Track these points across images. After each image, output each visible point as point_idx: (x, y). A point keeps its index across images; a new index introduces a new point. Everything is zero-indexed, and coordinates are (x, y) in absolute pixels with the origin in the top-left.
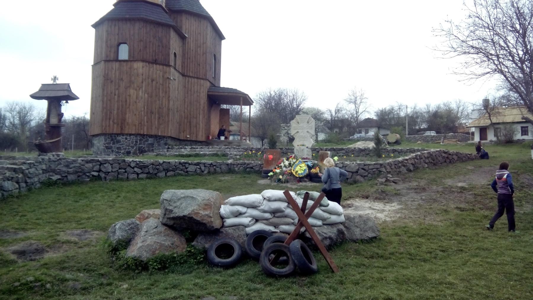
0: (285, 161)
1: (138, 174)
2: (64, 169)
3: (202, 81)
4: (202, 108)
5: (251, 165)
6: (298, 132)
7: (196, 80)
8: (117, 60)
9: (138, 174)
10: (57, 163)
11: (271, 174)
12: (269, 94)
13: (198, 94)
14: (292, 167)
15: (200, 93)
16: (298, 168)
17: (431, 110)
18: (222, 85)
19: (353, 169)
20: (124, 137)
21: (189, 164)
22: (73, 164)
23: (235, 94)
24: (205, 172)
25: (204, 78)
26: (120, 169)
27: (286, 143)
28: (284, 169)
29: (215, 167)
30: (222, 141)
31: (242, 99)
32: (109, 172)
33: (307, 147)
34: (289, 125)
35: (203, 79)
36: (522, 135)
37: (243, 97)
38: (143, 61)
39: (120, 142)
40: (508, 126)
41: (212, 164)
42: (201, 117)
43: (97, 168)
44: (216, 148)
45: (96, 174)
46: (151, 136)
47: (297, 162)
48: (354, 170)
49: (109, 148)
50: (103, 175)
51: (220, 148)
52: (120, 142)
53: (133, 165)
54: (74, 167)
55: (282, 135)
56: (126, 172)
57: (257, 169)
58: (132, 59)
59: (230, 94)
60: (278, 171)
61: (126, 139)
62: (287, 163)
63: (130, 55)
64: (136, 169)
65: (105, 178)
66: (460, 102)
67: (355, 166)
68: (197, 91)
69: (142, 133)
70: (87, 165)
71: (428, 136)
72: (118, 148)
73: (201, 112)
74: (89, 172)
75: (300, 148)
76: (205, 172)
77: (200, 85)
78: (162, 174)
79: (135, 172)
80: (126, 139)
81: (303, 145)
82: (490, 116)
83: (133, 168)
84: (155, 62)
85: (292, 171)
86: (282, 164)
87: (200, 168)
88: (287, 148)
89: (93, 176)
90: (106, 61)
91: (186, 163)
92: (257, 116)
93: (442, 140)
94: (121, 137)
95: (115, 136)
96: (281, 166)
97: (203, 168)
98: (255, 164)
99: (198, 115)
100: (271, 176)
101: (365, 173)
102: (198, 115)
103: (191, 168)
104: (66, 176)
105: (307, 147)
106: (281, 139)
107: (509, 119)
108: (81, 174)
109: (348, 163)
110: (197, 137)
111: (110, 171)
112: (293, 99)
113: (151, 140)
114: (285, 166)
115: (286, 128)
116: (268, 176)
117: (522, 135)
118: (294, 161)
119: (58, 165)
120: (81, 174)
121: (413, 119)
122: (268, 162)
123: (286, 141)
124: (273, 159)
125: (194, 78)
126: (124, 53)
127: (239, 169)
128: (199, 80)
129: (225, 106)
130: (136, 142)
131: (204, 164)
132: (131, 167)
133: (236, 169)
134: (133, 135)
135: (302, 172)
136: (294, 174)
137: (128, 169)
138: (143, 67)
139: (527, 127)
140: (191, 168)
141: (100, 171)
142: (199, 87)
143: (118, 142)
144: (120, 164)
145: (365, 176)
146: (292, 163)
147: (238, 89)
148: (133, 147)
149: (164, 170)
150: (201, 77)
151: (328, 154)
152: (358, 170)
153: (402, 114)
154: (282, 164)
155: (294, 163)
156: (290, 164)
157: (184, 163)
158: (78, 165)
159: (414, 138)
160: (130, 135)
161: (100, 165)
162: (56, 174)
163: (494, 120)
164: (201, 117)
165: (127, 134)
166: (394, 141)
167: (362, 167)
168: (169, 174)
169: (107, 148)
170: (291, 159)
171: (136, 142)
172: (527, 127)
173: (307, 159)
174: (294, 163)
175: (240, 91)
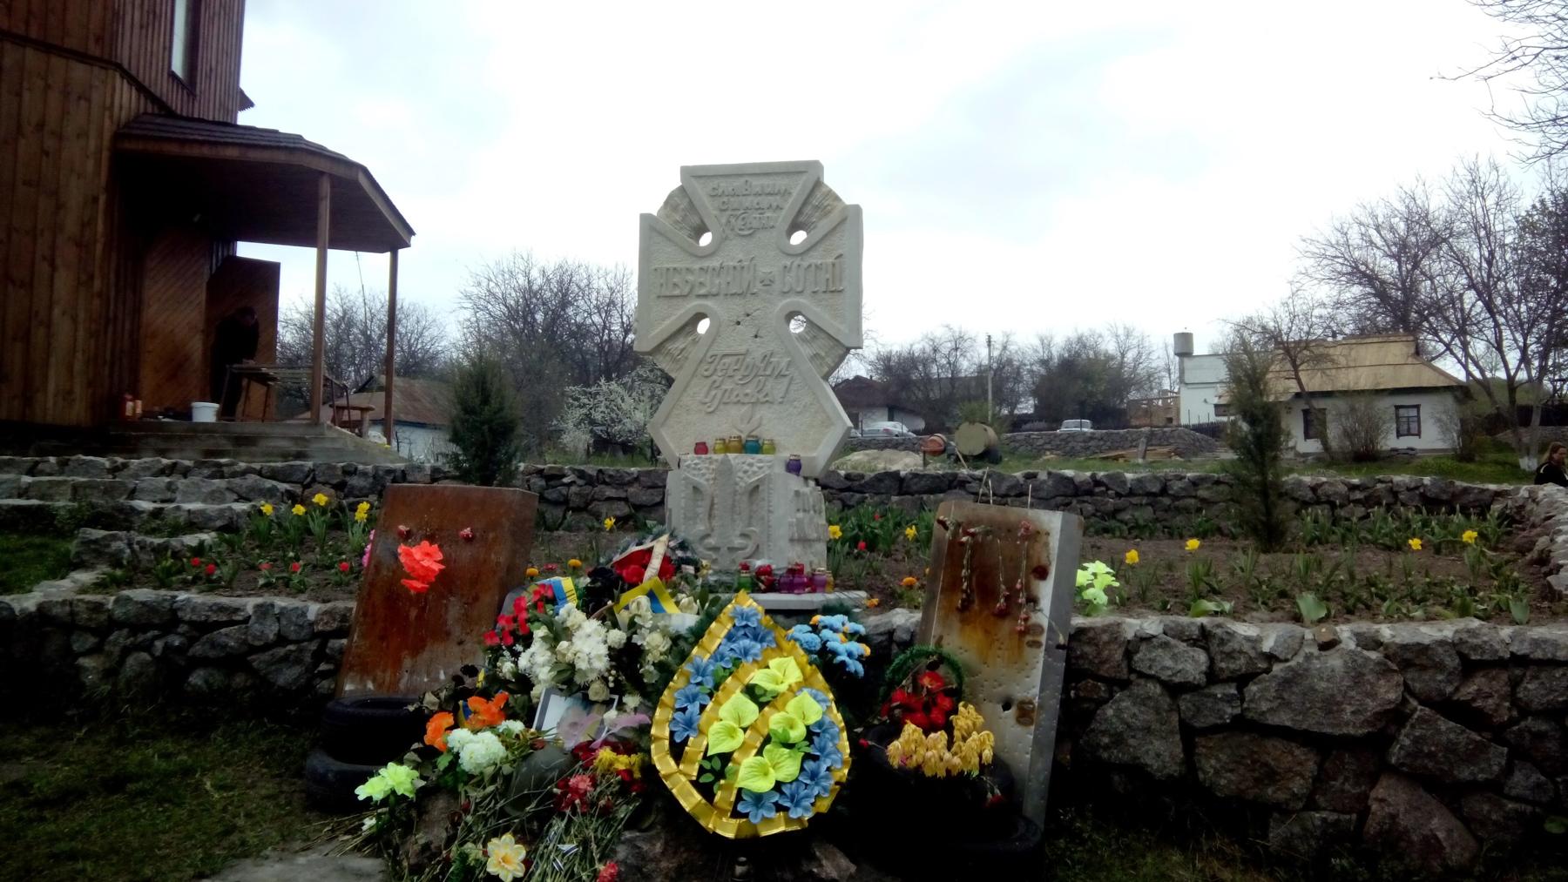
0: (569, 612)
3: (79, 71)
4: (71, 225)
5: (229, 637)
7: (32, 57)
11: (395, 778)
12: (522, 281)
13: (50, 143)
14: (651, 696)
15: (60, 137)
16: (726, 724)
17: (1055, 354)
19: (1331, 705)
23: (281, 157)
25: (94, 50)
27: (581, 454)
28: (556, 715)
30: (206, 428)
31: (325, 188)
33: (794, 467)
34: (593, 389)
35: (83, 57)
36: (1399, 435)
37: (337, 182)
40: (1361, 404)
42: (64, 281)
44: (86, 468)
47: (719, 631)
48: (1350, 722)
51: (115, 470)
55: (571, 426)
57: (288, 676)
59: (254, 155)
60: (477, 747)
62: (591, 644)
66: (1128, 336)
67: (1357, 675)
68: (41, 126)
71: (1072, 436)
73: (67, 253)
75: (726, 471)
77: (66, 94)
81: (752, 446)
82: (1296, 367)
85: (664, 763)
86: (536, 659)
88: (591, 469)
93: (1142, 447)
96: (524, 682)
98: (271, 630)
99: (44, 268)
101: (1474, 754)
102: (44, 268)
105: (794, 467)
106: (566, 439)
107: (1362, 379)
109: (1260, 633)
110: (28, 401)
112: (612, 303)
114: (569, 681)
115: (584, 400)
117: (1399, 435)
118: (682, 616)
121: (1000, 377)
122: (401, 618)
123: (582, 446)
124: (445, 582)
125: (23, 41)
127: (110, 673)
128: (57, 62)
129: (247, 250)
135: (788, 767)
136: (690, 800)
139: (1417, 407)
142: (54, 98)
145: (1473, 787)
146: (655, 644)
147: (309, 137)
150: (72, 43)
151: (1035, 535)
152: (1396, 716)
153: (966, 366)
154: (536, 659)
155: (681, 645)
156: (626, 658)
159: (1028, 441)
163: (1313, 382)
164: (64, 281)
166: (979, 450)
167: (1437, 682)
170: (636, 601)
172: (1417, 407)
173: (795, 579)
174: (681, 645)
175: (319, 152)
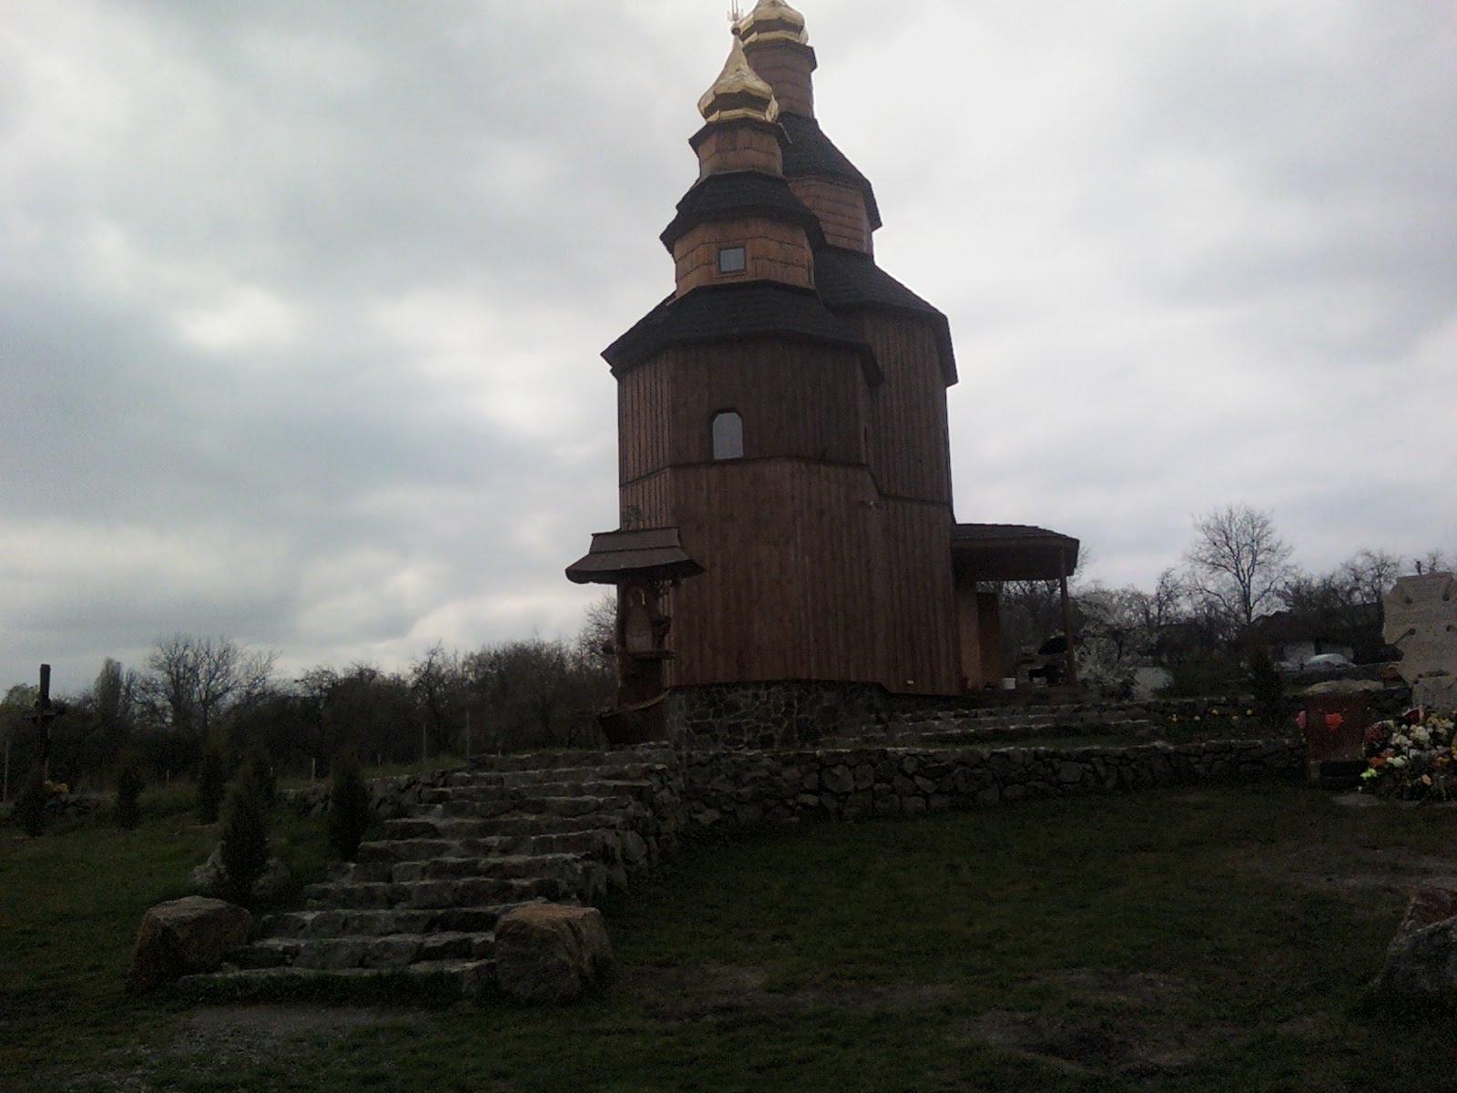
1: (926, 796)
2: (728, 788)
6: (1412, 632)
8: (711, 462)
9: (926, 796)
10: (708, 769)
11: (1370, 773)
18: (959, 521)
20: (750, 692)
21: (1063, 758)
22: (748, 769)
24: (1110, 784)
26: (877, 781)
29: (1134, 766)
32: (848, 794)
38: (792, 457)
39: (738, 709)
41: (1124, 755)
43: (811, 781)
45: (811, 800)
46: (830, 685)
49: (703, 731)
50: (832, 805)
52: (738, 709)
53: (909, 767)
54: (754, 780)
56: (893, 791)
58: (756, 451)
61: (756, 697)
63: (747, 441)
64: (919, 781)
65: (839, 812)
69: (805, 677)
70: (787, 773)
72: (731, 728)
74: (793, 797)
76: (1110, 784)
78: (991, 795)
79: (918, 788)
80: (756, 697)
83: (911, 777)
84: (823, 459)
87: (1095, 772)
89: (805, 806)
90: (675, 467)
91: (1054, 755)
92: (538, 651)
94: (741, 691)
95: (719, 692)
97: (1101, 769)
100: (1371, 779)
103: (1070, 773)
104: (733, 813)
108: (771, 802)
111: (850, 788)
113: (828, 699)
116: (1361, 782)
119: (712, 776)
120: (771, 802)
126: (728, 436)
129: (984, 586)
130: (790, 705)
131: (1103, 756)
132: (905, 774)
133: (1200, 768)
134: (777, 683)
137: (899, 781)
138: (792, 475)
140: (1070, 773)
141: (820, 790)
143: (732, 708)
144: (874, 765)
148: (778, 723)
149: (995, 779)
157: (1046, 754)
158: (764, 773)
160: (768, 684)
161: (819, 772)
162: (709, 806)
165: (757, 684)
168: (1010, 792)
169: (699, 730)
171: (790, 705)
